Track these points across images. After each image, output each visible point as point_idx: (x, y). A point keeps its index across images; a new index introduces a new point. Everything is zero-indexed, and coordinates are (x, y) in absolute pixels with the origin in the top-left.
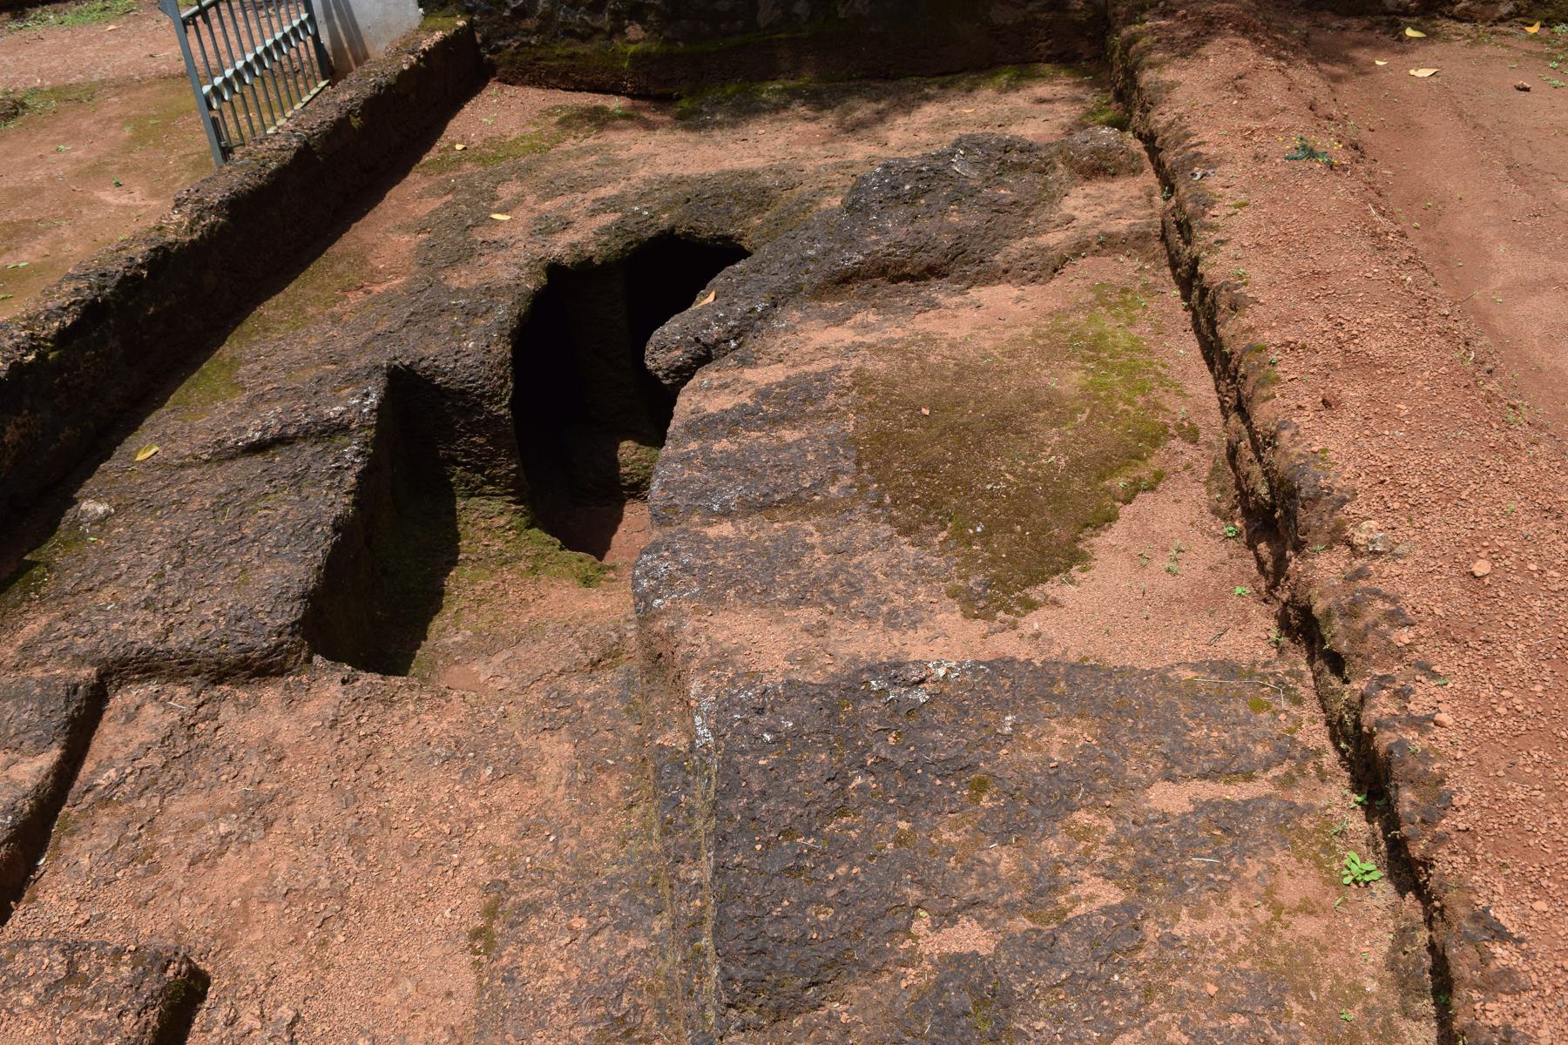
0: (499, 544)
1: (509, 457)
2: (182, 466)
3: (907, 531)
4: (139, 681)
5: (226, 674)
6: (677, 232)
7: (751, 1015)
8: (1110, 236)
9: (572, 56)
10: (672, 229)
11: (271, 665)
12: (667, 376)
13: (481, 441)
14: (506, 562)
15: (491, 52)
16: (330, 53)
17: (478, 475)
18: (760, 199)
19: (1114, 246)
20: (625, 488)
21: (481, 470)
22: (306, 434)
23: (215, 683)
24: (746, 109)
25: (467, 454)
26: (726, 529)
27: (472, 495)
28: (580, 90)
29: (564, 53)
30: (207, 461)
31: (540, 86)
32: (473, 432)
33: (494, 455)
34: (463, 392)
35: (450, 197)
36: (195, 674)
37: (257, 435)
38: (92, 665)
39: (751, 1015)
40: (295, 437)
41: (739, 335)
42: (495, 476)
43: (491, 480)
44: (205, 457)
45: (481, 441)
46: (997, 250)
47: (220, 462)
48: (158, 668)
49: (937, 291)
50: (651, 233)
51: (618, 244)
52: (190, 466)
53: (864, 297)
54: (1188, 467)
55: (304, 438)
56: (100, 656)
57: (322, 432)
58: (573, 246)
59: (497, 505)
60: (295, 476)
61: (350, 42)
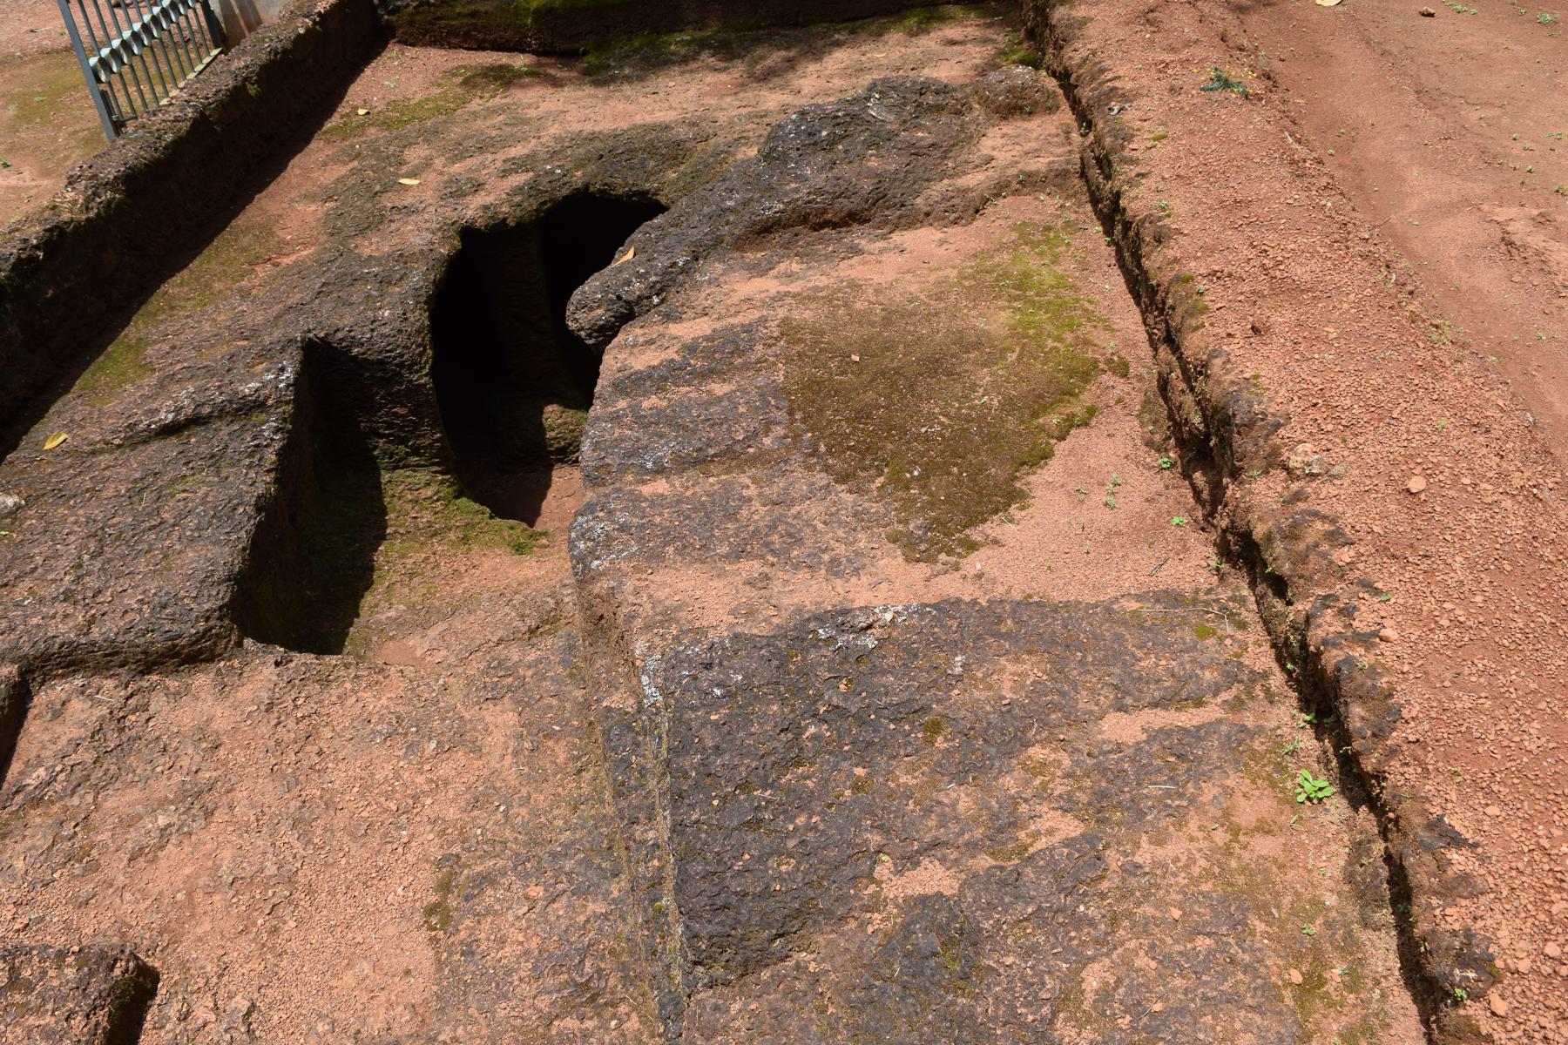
0: (427, 516)
1: (433, 426)
2: (93, 453)
3: (843, 478)
4: (63, 676)
5: (154, 664)
6: (592, 189)
7: (718, 971)
8: (1029, 175)
9: (473, 14)
10: (587, 187)
11: (200, 651)
12: (590, 336)
13: (403, 411)
14: (435, 534)
15: (389, 13)
16: (221, 19)
17: (402, 447)
18: (675, 152)
19: (1034, 184)
20: (552, 453)
21: (404, 441)
22: (222, 413)
23: (143, 673)
24: (654, 62)
25: (389, 426)
26: (660, 486)
27: (397, 467)
28: (484, 49)
29: (465, 11)
30: (119, 446)
31: (442, 47)
32: (395, 404)
33: (416, 426)
34: (381, 362)
35: (355, 163)
36: (122, 666)
37: (170, 416)
38: (13, 662)
39: (718, 971)
40: (210, 416)
41: (662, 290)
42: (419, 447)
43: (416, 451)
44: (117, 442)
45: (403, 411)
46: (918, 194)
47: (133, 446)
48: (82, 661)
49: (858, 236)
50: (565, 192)
51: (533, 204)
52: (102, 452)
53: (786, 246)
54: (1119, 401)
55: (220, 417)
56: (21, 653)
57: (237, 410)
58: (486, 208)
59: (423, 476)
60: (213, 456)
61: (241, 7)
